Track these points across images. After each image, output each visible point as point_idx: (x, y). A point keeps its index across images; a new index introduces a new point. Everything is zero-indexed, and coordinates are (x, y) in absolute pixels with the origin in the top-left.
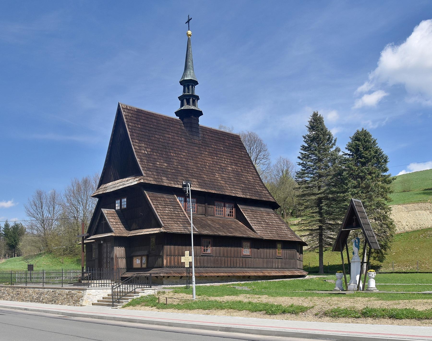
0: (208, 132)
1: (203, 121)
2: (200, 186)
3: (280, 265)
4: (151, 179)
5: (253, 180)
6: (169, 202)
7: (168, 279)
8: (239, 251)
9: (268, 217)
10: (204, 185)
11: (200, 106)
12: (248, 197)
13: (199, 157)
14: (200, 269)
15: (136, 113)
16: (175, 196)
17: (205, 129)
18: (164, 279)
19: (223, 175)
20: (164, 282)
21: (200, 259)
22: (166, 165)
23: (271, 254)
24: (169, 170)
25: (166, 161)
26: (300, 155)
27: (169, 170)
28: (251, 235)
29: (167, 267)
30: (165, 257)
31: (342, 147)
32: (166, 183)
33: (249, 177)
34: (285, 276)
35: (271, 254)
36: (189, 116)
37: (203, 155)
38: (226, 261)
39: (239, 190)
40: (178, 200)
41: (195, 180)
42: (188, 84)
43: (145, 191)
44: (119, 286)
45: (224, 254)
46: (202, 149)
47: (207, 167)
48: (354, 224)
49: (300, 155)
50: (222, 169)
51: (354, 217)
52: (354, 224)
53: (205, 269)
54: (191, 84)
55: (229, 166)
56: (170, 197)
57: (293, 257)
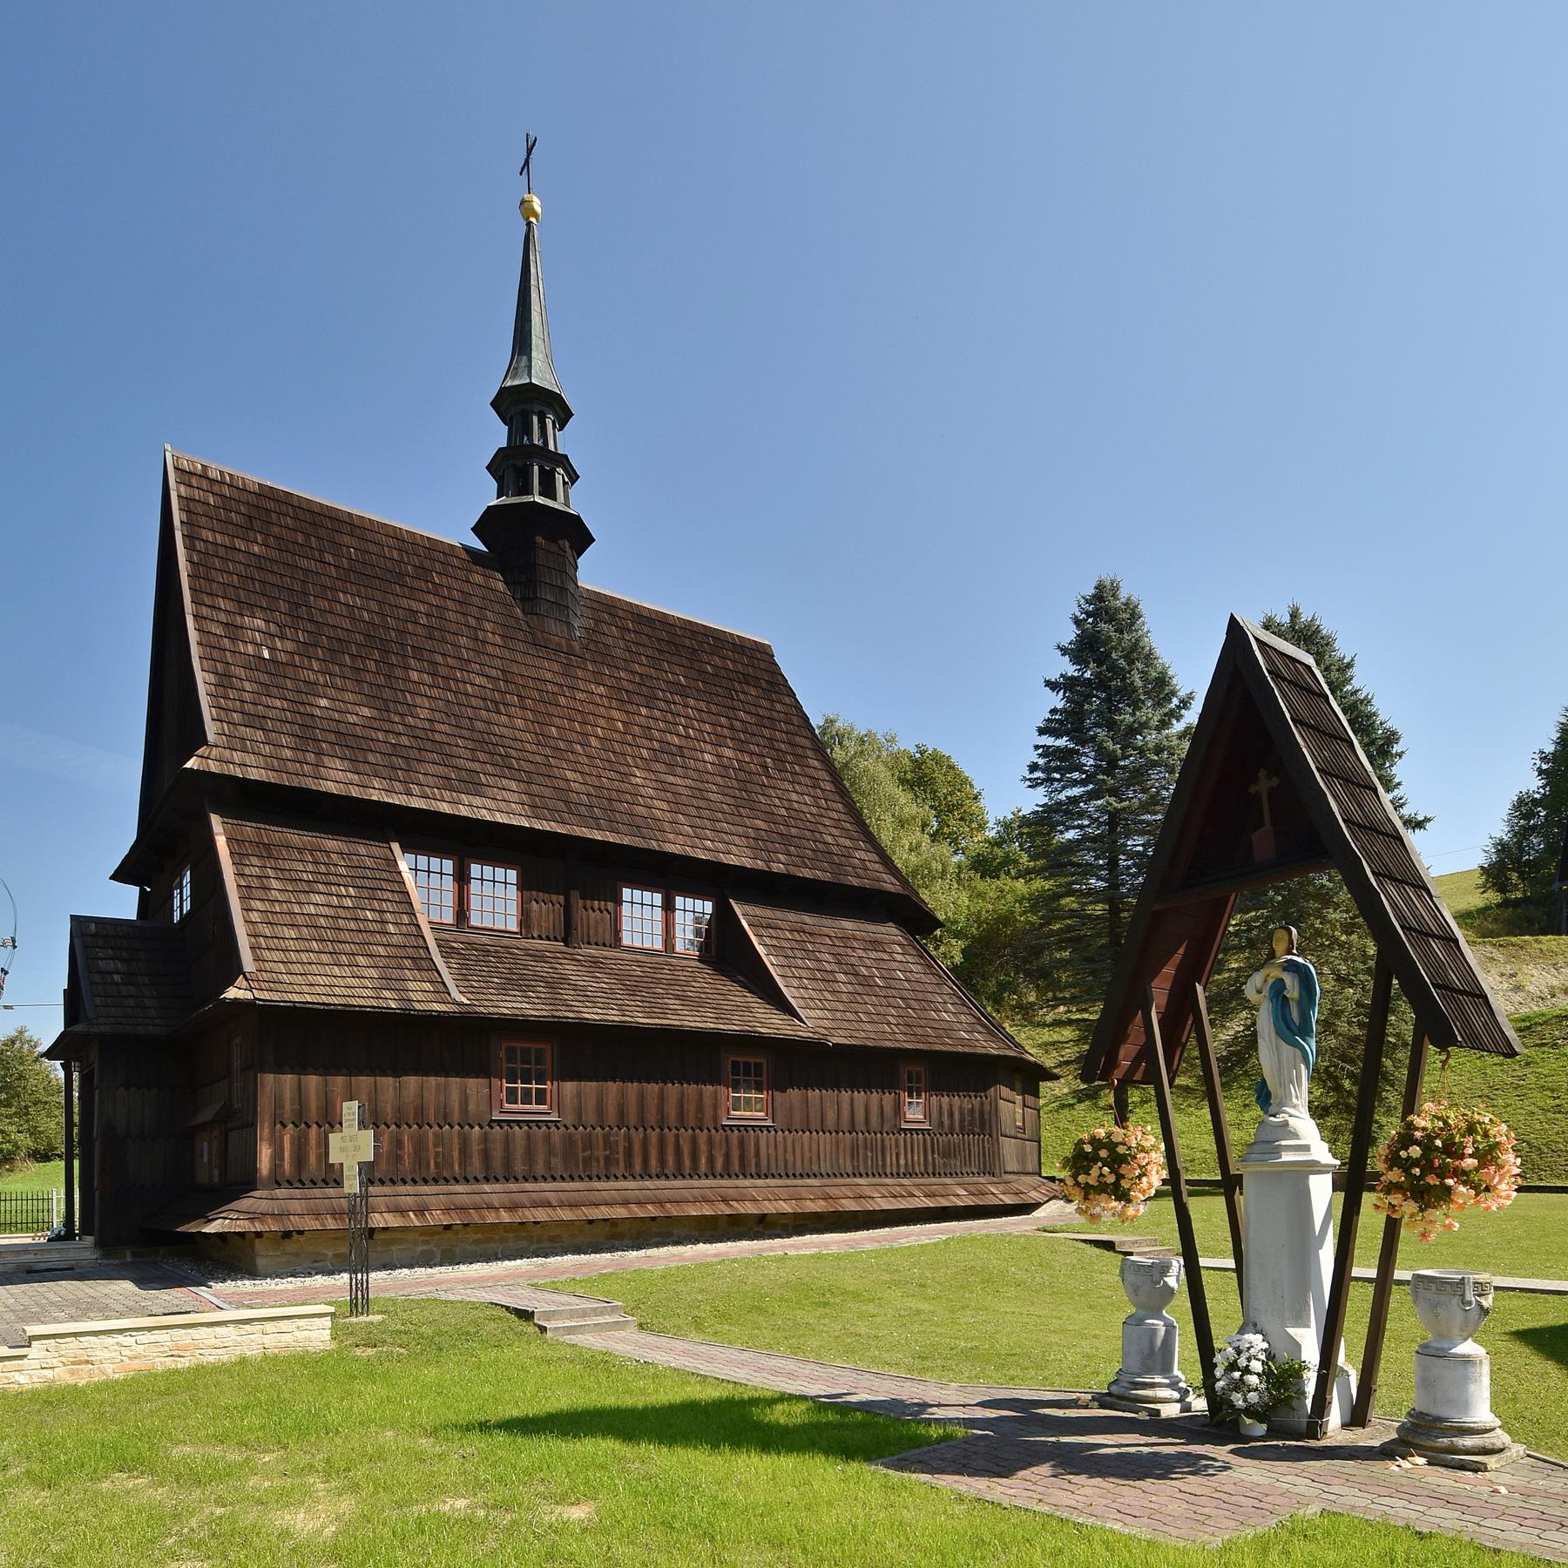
0: (621, 613)
1: (594, 573)
2: (536, 810)
3: (918, 1157)
4: (250, 759)
5: (814, 810)
6: (343, 871)
7: (289, 1246)
8: (707, 1101)
9: (873, 955)
10: (561, 806)
11: (577, 501)
12: (777, 868)
13: (562, 700)
14: (487, 1188)
15: (252, 499)
16: (395, 846)
17: (606, 607)
18: (258, 1244)
19: (671, 779)
20: (261, 1262)
21: (485, 1139)
22: (366, 712)
23: (874, 1109)
24: (381, 736)
25: (371, 700)
26: (1034, 757)
27: (381, 736)
28: (769, 1022)
29: (276, 1181)
30: (264, 1130)
31: (1192, 670)
32: (336, 779)
33: (794, 797)
34: (762, 1218)
35: (874, 1109)
36: (530, 537)
37: (579, 696)
38: (637, 1147)
39: (737, 840)
40: (403, 866)
41: (513, 785)
42: (526, 406)
43: (215, 820)
44: (1500, 1167)
45: (622, 1114)
46: (580, 673)
47: (594, 742)
48: (1263, 842)
49: (1034, 757)
50: (671, 756)
51: (1264, 784)
52: (1263, 842)
53: (445, 1188)
54: (537, 408)
55: (709, 747)
56: (363, 849)
57: (984, 1124)
